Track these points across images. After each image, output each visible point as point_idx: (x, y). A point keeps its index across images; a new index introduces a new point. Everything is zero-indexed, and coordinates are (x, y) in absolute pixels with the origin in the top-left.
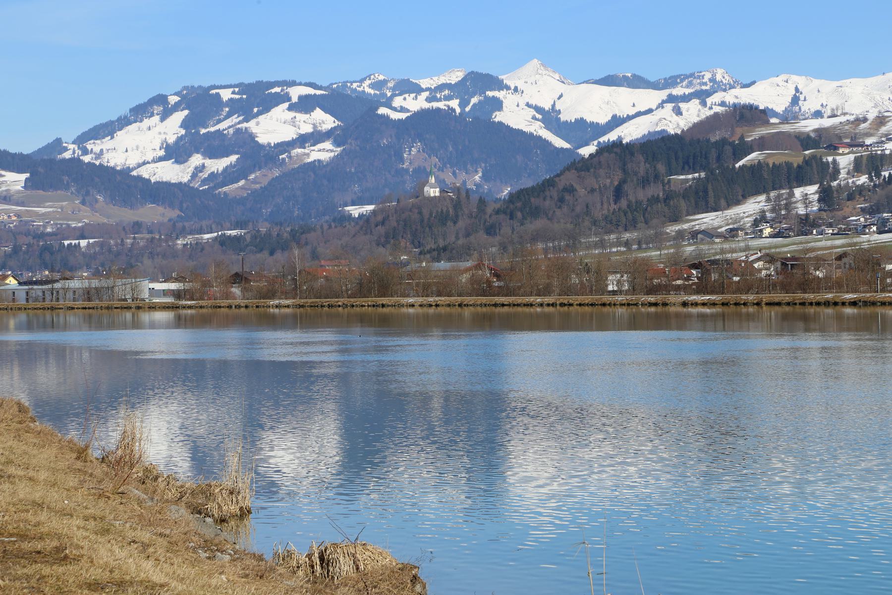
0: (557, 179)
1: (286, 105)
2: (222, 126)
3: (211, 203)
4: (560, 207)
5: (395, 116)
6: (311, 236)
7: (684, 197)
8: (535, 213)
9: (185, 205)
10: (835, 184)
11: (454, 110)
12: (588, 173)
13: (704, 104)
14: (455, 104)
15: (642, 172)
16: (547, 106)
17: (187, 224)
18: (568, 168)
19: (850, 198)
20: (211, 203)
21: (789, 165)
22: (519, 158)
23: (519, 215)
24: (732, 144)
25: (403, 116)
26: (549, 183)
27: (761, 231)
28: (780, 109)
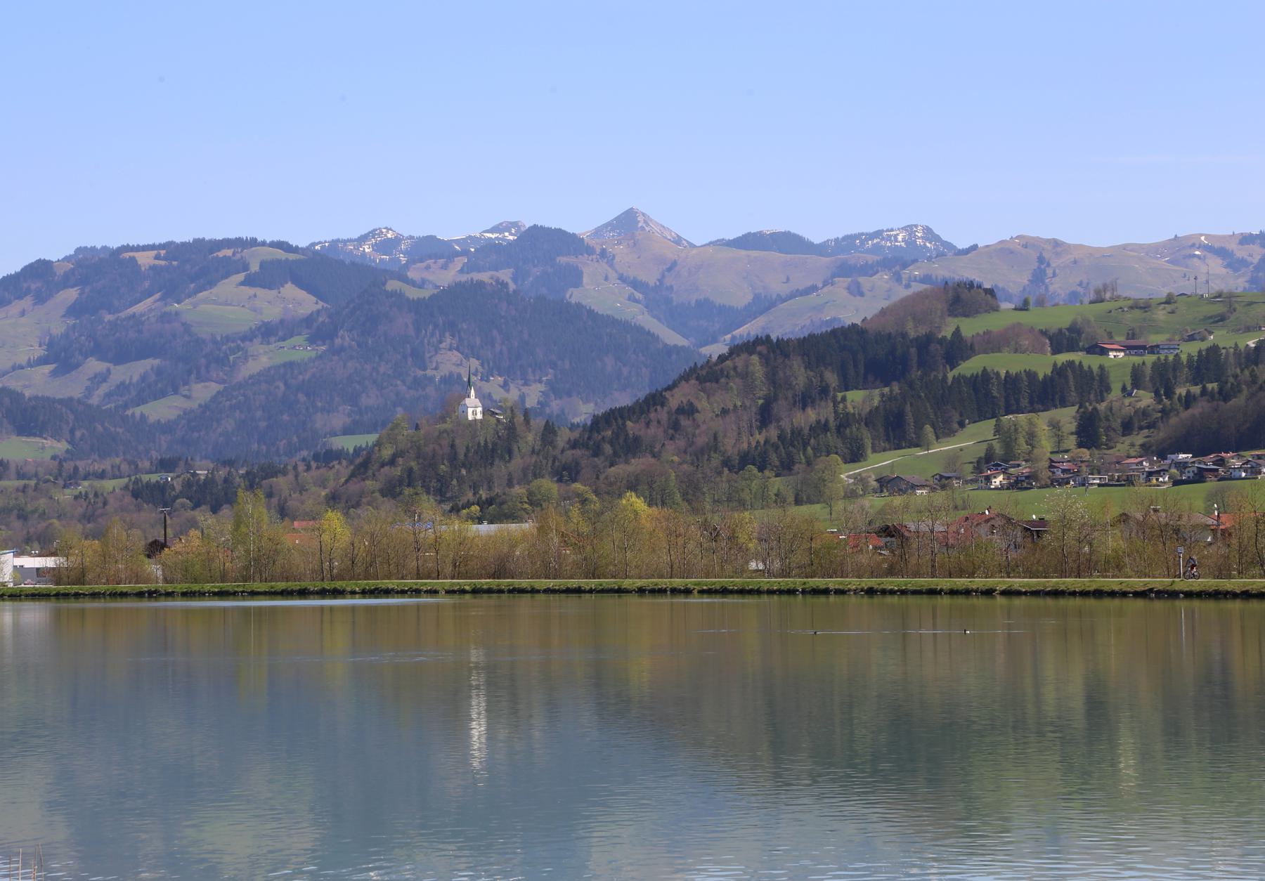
0: (667, 394)
1: (241, 277)
2: (139, 308)
3: (120, 430)
5: (413, 293)
6: (282, 483)
7: (866, 425)
9: (78, 434)
10: (1102, 407)
11: (504, 285)
12: (714, 385)
13: (898, 278)
14: (505, 275)
16: (651, 278)
17: (81, 465)
18: (685, 377)
19: (1127, 427)
20: (120, 430)
21: (1031, 375)
23: (608, 449)
25: (425, 294)
26: (655, 400)
27: (988, 479)
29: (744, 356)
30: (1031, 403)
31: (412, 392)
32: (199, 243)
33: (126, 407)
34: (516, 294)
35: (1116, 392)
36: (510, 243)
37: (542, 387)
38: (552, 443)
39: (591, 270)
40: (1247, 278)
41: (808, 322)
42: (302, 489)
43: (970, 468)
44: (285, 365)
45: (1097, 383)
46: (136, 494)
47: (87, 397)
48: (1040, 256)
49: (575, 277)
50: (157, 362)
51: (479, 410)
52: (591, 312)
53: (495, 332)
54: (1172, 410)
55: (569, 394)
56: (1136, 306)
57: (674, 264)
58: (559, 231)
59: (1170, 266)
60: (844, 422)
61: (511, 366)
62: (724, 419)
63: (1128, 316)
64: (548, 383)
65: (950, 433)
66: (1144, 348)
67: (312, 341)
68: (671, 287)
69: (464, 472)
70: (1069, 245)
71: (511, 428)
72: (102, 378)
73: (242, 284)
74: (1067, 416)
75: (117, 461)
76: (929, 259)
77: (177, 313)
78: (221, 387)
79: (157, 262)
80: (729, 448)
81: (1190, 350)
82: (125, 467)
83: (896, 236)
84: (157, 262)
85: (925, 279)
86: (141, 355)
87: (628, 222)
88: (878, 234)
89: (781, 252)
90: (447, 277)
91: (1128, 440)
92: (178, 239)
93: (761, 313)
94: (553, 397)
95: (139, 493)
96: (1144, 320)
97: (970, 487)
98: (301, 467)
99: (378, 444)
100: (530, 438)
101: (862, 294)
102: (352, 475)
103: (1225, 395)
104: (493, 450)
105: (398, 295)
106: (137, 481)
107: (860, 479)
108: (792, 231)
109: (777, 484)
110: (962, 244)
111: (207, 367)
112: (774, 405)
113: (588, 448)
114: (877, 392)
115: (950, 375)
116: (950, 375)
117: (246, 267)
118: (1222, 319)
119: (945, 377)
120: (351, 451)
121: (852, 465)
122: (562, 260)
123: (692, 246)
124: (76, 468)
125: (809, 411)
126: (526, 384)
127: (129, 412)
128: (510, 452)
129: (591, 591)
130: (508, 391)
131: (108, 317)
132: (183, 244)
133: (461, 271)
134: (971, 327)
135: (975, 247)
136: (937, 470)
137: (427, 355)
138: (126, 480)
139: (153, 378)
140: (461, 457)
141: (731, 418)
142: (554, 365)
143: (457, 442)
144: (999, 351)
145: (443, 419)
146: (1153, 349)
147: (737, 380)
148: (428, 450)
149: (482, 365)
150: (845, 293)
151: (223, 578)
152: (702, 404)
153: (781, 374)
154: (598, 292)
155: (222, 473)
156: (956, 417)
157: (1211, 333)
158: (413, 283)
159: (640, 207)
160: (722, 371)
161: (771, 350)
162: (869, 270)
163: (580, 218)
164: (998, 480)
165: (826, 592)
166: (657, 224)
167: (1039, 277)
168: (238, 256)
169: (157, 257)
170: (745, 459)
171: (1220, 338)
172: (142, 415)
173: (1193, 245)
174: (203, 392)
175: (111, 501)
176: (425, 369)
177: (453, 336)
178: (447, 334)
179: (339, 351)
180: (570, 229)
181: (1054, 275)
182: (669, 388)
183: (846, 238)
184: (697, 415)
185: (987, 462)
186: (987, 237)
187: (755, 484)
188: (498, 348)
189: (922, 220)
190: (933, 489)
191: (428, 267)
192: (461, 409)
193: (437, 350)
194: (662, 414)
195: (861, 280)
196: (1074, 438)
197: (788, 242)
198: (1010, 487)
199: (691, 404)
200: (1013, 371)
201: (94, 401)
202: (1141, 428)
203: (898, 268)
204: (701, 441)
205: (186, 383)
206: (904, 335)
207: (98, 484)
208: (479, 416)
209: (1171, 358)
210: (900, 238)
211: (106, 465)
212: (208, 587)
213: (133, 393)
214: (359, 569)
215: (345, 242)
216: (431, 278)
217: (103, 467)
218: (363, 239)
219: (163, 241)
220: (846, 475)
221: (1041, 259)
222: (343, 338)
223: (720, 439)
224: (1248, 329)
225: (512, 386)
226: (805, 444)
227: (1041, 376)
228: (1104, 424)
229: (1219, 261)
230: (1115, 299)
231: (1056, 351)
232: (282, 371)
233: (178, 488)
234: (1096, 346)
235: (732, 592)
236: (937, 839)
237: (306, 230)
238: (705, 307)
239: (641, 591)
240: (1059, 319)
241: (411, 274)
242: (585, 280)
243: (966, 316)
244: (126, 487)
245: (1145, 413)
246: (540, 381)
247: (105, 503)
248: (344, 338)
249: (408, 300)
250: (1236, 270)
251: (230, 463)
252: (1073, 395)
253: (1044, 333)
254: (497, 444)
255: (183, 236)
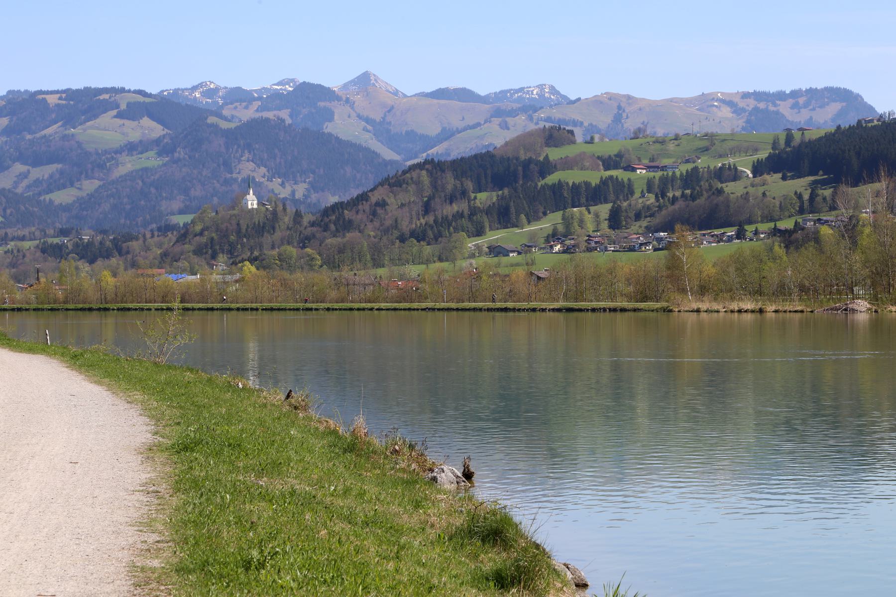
0: (370, 194)
1: (115, 112)
2: (48, 131)
3: (36, 209)
4: (372, 221)
5: (224, 125)
6: (135, 245)
7: (487, 214)
8: (348, 226)
9: (8, 211)
10: (625, 204)
11: (283, 121)
12: (399, 189)
13: (531, 118)
14: (285, 114)
15: (450, 187)
16: (378, 117)
17: (9, 231)
18: (381, 184)
19: (638, 217)
20: (36, 209)
21: (587, 184)
22: (348, 169)
23: (332, 227)
24: (537, 163)
25: (232, 125)
26: (363, 197)
27: (552, 247)
28: (602, 127)
29: (418, 171)
30: (587, 200)
31: (223, 188)
32: (87, 90)
33: (40, 194)
34: (290, 128)
35: (637, 194)
36: (289, 92)
37: (306, 186)
38: (299, 223)
39: (340, 111)
40: (744, 120)
41: (474, 146)
42: (147, 249)
43: (542, 240)
44: (142, 169)
45: (625, 189)
46: (43, 251)
47: (14, 188)
48: (619, 106)
49: (329, 116)
50: (60, 166)
51: (255, 202)
52: (337, 138)
53: (276, 151)
54: (664, 206)
55: (323, 191)
56: (656, 142)
57: (392, 107)
58: (320, 86)
59: (699, 113)
60: (474, 211)
61: (287, 172)
62: (402, 209)
63: (652, 147)
64: (310, 183)
65: (538, 219)
66: (657, 167)
67: (159, 154)
68: (390, 123)
69: (245, 240)
70: (637, 99)
71: (274, 213)
72: (25, 175)
73: (116, 117)
74: (604, 210)
75: (33, 229)
76: (551, 106)
77: (73, 135)
78: (101, 183)
79: (60, 102)
80: (404, 227)
81: (684, 168)
82: (37, 233)
83: (532, 91)
84: (60, 102)
85: (548, 119)
86: (51, 160)
87: (364, 80)
88: (521, 90)
89: (460, 101)
90: (247, 114)
91: (638, 224)
92: (74, 87)
93: (446, 140)
94: (312, 191)
95: (45, 250)
96: (662, 150)
97: (542, 251)
98: (148, 235)
99: (193, 222)
100: (287, 220)
101: (508, 129)
102: (177, 241)
103: (693, 198)
104: (263, 227)
105: (215, 126)
106: (45, 243)
107: (478, 247)
108: (467, 87)
109: (428, 250)
110: (573, 98)
111: (93, 170)
112: (432, 202)
113: (321, 227)
114: (494, 194)
115: (539, 184)
116: (539, 184)
117: (118, 106)
118: (706, 149)
119: (536, 184)
120: (181, 225)
121: (477, 238)
122: (321, 104)
123: (405, 96)
124: (6, 234)
125: (454, 205)
126: (295, 184)
127: (42, 198)
128: (274, 228)
129: (217, 309)
130: (284, 188)
131: (28, 137)
132: (77, 90)
133: (257, 110)
134: (555, 154)
135: (579, 99)
136: (525, 241)
137: (233, 165)
138: (38, 242)
139: (58, 176)
140: (244, 231)
141: (406, 209)
142: (314, 172)
143: (241, 222)
144: (572, 169)
145: (233, 208)
146: (663, 168)
147: (413, 186)
148: (223, 226)
149: (268, 171)
150: (497, 128)
151: (55, 302)
152: (391, 200)
153: (439, 182)
154: (344, 126)
155: (99, 238)
156: (542, 210)
157: (699, 158)
158: (225, 119)
159: (373, 71)
160: (404, 180)
161: (434, 167)
162: (513, 113)
163: (333, 76)
164: (557, 248)
165: (311, 309)
166: (382, 81)
167: (618, 119)
168: (113, 99)
169: (60, 99)
170: (413, 234)
171: (702, 163)
172: (50, 200)
173: (713, 99)
174: (89, 186)
175: (28, 255)
176: (232, 173)
177: (250, 152)
178: (246, 152)
179: (176, 161)
180: (326, 85)
181: (627, 117)
182: (372, 190)
183: (501, 92)
184: (387, 207)
185: (554, 236)
186: (586, 93)
187: (415, 250)
188: (278, 160)
189: (548, 82)
190: (519, 253)
191: (236, 108)
192: (244, 201)
193: (240, 161)
194: (366, 206)
195: (508, 119)
196: (606, 222)
197: (464, 95)
198: (564, 252)
199: (384, 200)
200: (577, 182)
201: (19, 190)
202: (646, 217)
203: (531, 112)
204: (388, 223)
205: (79, 180)
206: (517, 159)
207: (20, 244)
208: (255, 206)
209: (670, 174)
210: (535, 92)
211: (26, 232)
212: (46, 306)
213: (45, 185)
214: (119, 299)
215: (183, 90)
216: (237, 115)
217: (23, 233)
218: (195, 88)
219: (64, 88)
220: (471, 244)
221: (619, 107)
222: (179, 153)
223: (399, 221)
224: (721, 156)
225: (287, 185)
226: (450, 225)
227: (593, 185)
228: (624, 214)
229: (729, 109)
230: (646, 137)
231: (607, 168)
232: (140, 173)
233: (70, 247)
234: (629, 166)
235: (275, 309)
236: (604, 484)
237: (156, 83)
238: (411, 135)
239: (238, 309)
240: (610, 149)
241: (226, 112)
242: (336, 117)
243: (556, 146)
244: (37, 247)
245: (649, 208)
246: (305, 182)
247: (24, 256)
248: (180, 153)
249: (221, 129)
250: (739, 115)
251: (104, 232)
252: (612, 197)
253: (599, 158)
254: (266, 224)
255: (77, 84)
